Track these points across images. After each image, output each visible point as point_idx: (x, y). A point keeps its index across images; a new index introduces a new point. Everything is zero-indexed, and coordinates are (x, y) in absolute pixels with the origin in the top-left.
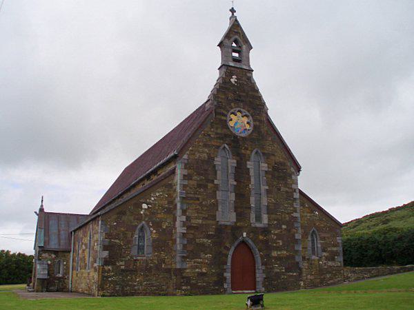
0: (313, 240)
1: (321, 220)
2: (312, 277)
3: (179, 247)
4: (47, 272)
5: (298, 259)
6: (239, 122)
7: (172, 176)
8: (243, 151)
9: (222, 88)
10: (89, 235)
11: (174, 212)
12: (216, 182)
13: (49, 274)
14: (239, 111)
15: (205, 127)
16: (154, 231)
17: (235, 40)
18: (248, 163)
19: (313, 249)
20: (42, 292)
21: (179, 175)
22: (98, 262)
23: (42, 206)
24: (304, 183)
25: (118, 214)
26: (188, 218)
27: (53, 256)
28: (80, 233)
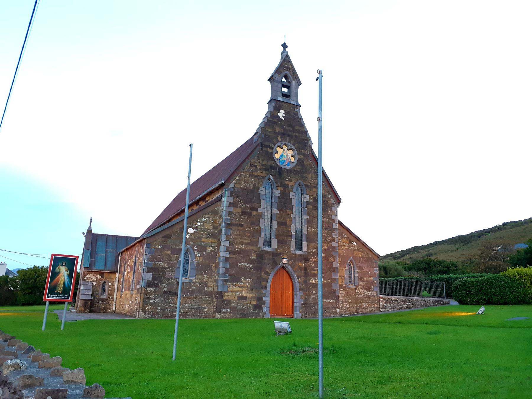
0: (350, 270)
1: (359, 250)
2: (349, 305)
3: (222, 271)
4: (91, 293)
5: (335, 287)
6: (285, 155)
7: (219, 203)
8: (287, 183)
9: (271, 121)
10: (134, 257)
11: (218, 237)
12: (260, 210)
13: (92, 295)
14: (285, 145)
15: (254, 154)
16: (199, 255)
17: (285, 76)
18: (291, 193)
19: (351, 278)
20: (84, 312)
21: (225, 202)
22: (141, 283)
23: (90, 227)
24: (344, 214)
25: (163, 237)
26: (231, 244)
27: (99, 277)
28: (127, 255)
